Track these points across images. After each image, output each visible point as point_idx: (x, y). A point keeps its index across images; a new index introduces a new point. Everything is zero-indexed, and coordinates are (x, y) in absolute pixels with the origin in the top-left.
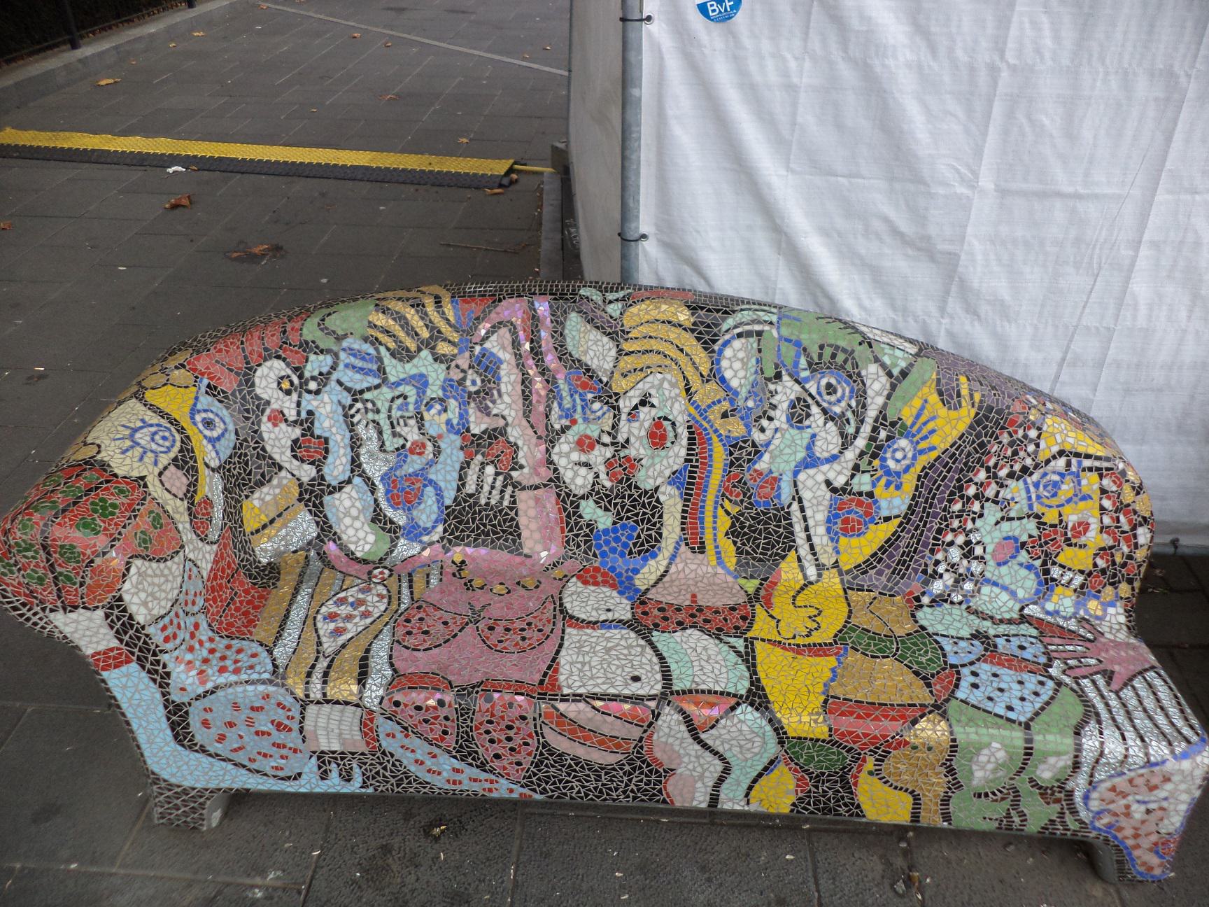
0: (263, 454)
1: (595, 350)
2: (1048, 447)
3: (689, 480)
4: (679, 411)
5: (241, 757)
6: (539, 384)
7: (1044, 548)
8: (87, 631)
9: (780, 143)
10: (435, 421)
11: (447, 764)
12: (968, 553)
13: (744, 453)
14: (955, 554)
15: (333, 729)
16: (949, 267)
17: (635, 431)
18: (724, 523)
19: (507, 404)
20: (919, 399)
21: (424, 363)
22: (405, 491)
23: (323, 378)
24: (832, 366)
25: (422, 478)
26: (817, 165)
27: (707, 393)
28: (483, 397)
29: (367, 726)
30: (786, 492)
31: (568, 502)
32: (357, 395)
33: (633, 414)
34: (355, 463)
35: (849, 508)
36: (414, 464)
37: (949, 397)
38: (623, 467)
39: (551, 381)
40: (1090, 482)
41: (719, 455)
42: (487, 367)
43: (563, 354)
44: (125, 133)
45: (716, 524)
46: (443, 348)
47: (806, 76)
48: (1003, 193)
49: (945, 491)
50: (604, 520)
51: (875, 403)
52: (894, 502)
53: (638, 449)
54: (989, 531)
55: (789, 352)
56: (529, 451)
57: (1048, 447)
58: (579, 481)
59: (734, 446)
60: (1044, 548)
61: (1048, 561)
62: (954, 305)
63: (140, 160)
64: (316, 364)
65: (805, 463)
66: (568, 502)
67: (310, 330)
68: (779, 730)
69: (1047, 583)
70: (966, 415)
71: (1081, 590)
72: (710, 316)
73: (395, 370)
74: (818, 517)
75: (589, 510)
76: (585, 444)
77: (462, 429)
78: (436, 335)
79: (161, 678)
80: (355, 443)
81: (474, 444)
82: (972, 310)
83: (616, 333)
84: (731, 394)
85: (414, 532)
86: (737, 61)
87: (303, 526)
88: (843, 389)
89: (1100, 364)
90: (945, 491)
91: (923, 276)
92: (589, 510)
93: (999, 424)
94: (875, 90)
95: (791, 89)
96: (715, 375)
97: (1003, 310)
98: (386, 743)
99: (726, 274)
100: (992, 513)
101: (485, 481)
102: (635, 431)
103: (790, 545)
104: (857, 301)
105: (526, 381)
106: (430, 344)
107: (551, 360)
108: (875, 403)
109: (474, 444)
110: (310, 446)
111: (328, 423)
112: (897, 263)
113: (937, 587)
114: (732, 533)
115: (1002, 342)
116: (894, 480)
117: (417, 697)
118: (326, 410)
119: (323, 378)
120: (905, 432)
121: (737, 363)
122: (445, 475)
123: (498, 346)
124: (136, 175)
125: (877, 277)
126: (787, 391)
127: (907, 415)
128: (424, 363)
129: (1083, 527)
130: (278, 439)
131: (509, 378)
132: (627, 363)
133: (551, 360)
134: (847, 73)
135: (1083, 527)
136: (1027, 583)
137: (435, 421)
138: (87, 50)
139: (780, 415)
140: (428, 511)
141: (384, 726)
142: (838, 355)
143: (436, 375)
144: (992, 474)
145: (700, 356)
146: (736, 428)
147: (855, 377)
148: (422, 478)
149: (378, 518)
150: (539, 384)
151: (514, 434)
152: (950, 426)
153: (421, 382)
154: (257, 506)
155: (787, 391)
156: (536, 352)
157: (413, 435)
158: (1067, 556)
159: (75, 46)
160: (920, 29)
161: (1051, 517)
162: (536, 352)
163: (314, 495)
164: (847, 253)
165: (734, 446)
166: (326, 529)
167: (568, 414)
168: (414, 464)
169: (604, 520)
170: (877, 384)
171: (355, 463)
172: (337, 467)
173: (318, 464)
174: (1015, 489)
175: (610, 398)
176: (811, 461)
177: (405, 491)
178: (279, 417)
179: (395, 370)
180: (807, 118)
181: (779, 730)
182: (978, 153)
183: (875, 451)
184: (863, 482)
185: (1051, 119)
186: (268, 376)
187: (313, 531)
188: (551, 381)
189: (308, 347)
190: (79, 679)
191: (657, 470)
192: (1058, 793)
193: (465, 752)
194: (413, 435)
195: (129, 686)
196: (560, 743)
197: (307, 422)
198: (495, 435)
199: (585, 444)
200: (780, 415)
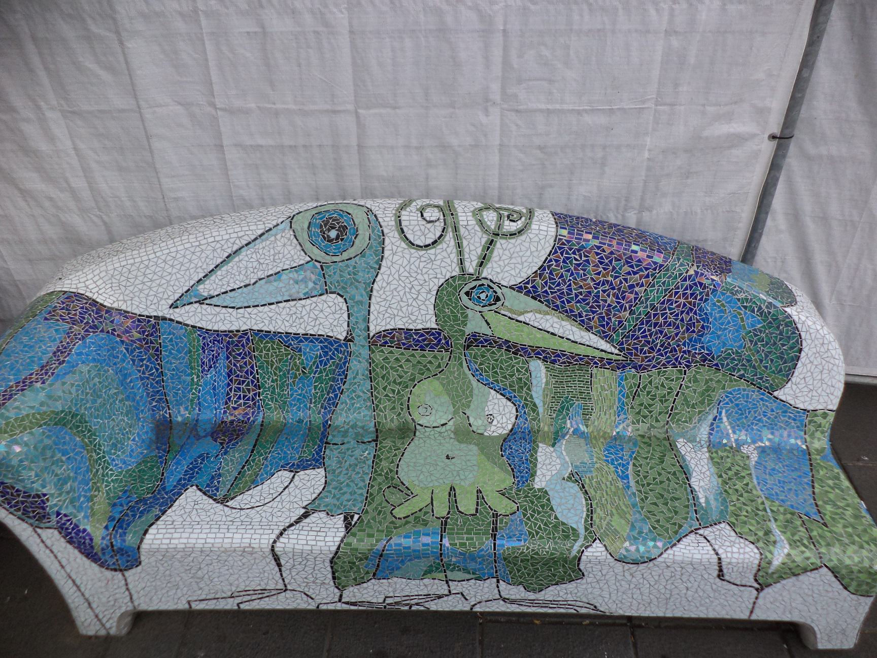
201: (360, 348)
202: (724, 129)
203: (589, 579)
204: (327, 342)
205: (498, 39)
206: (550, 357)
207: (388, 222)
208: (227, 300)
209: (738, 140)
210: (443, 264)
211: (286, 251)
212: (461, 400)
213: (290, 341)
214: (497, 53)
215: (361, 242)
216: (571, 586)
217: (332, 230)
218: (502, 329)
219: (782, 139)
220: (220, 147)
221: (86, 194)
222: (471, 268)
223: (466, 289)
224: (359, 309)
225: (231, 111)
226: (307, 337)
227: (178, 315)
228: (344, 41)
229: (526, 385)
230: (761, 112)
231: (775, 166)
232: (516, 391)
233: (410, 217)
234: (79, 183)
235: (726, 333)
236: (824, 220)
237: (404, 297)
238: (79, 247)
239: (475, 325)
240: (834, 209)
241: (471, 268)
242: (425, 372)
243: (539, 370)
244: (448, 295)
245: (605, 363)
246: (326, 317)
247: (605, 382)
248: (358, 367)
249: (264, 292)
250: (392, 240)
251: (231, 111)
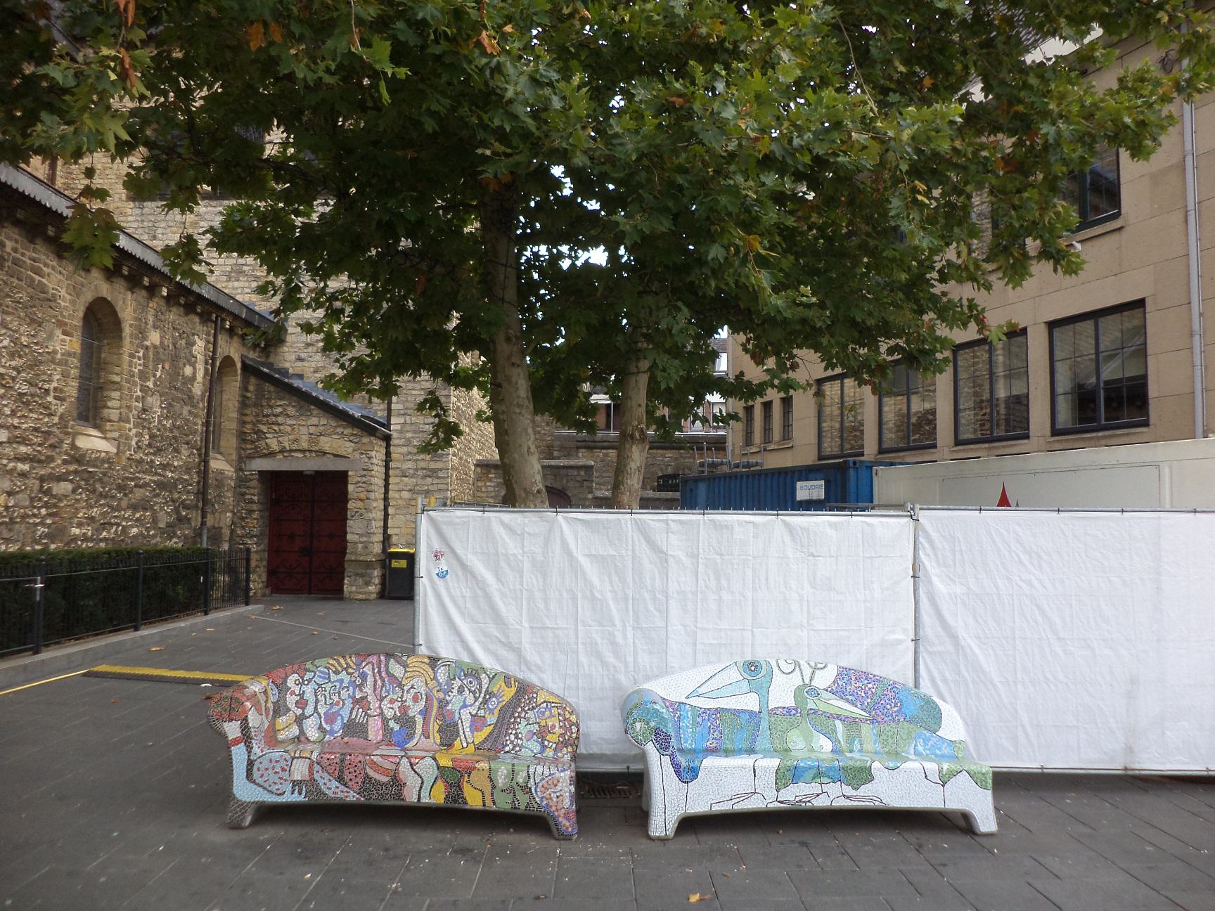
0: (286, 706)
1: (397, 670)
2: (540, 700)
3: (425, 713)
4: (423, 690)
5: (266, 785)
6: (379, 683)
7: (542, 733)
8: (232, 729)
9: (462, 614)
10: (344, 694)
11: (335, 783)
12: (517, 738)
13: (443, 704)
14: (512, 737)
15: (300, 771)
16: (517, 651)
17: (408, 697)
18: (437, 727)
19: (368, 689)
20: (499, 684)
21: (343, 675)
22: (331, 718)
23: (310, 680)
24: (471, 675)
25: (337, 714)
26: (474, 621)
27: (432, 684)
28: (361, 687)
29: (311, 768)
30: (457, 716)
31: (385, 721)
32: (320, 686)
33: (408, 691)
34: (316, 708)
35: (477, 722)
36: (336, 708)
37: (508, 685)
38: (404, 709)
39: (383, 681)
40: (555, 711)
41: (435, 704)
42: (363, 677)
43: (388, 672)
44: (176, 669)
45: (434, 727)
46: (350, 670)
47: (468, 594)
48: (532, 628)
49: (508, 715)
50: (397, 728)
51: (485, 687)
52: (491, 719)
53: (409, 703)
54: (523, 729)
55: (458, 671)
56: (374, 704)
57: (540, 700)
58: (389, 714)
59: (440, 701)
60: (542, 733)
61: (543, 739)
62: (523, 667)
63: (184, 681)
64: (309, 675)
65: (463, 708)
66: (385, 721)
67: (309, 665)
68: (438, 765)
69: (544, 747)
70: (514, 690)
71: (555, 750)
72: (434, 661)
73: (333, 677)
74: (467, 725)
75: (392, 724)
76: (392, 702)
77: (353, 697)
78: (349, 666)
79: (249, 749)
80: (317, 701)
81: (356, 702)
82: (530, 669)
83: (405, 666)
84: (440, 684)
85: (332, 732)
86: (448, 589)
87: (295, 731)
88: (475, 682)
89: (578, 689)
90: (508, 715)
91: (511, 656)
92: (392, 724)
93: (524, 690)
94: (488, 598)
95: (464, 597)
96: (435, 678)
97: (539, 668)
98: (316, 776)
99: (445, 652)
100: (524, 722)
101: (359, 715)
102: (408, 697)
103: (458, 735)
104: (487, 662)
105: (375, 681)
106: (346, 669)
107: (384, 674)
108: (485, 687)
109: (356, 702)
110: (302, 703)
111: (309, 695)
112: (503, 652)
113: (507, 749)
114: (439, 731)
115: (541, 679)
116: (491, 712)
117: (328, 756)
118: (309, 691)
119: (310, 680)
120: (495, 696)
121: (442, 675)
122: (345, 713)
123: (368, 670)
124: (182, 687)
125: (498, 659)
126: (457, 683)
127: (495, 690)
128: (343, 675)
129: (553, 726)
130: (291, 700)
131: (370, 680)
132: (408, 674)
133: (384, 674)
134: (479, 592)
135: (553, 726)
136: (537, 748)
137: (344, 694)
138: (145, 632)
139: (455, 691)
140: (338, 725)
141: (317, 767)
142: (474, 672)
143: (347, 679)
144: (523, 710)
145: (431, 672)
146: (441, 695)
147: (478, 679)
148: (337, 714)
149: (320, 728)
150: (379, 683)
151: (369, 698)
152: (509, 693)
153: (341, 681)
154: (281, 721)
155: (457, 683)
156: (379, 672)
157: (336, 698)
158: (549, 737)
159: (136, 629)
160: (499, 580)
161: (543, 723)
162: (379, 672)
163: (300, 720)
164: (486, 649)
165: (440, 701)
166: (302, 731)
167: (387, 691)
168: (336, 708)
169: (397, 728)
170: (485, 681)
171: (316, 708)
172: (309, 710)
173: (303, 709)
174: (530, 714)
175: (401, 686)
176: (465, 706)
177: (331, 718)
178: (293, 693)
179: (333, 677)
180: (469, 605)
181: (438, 765)
182: (521, 615)
183: (485, 702)
184: (481, 713)
185: (541, 605)
186: (291, 681)
187: (297, 733)
188: (383, 681)
189: (307, 670)
190: (226, 745)
191: (415, 710)
192: (525, 789)
193: (340, 779)
194: (336, 698)
195: (239, 754)
196: (371, 773)
197: (302, 695)
198: (364, 698)
199: (392, 702)
200: (455, 691)
201: (765, 715)
202: (892, 637)
203: (876, 780)
204: (751, 713)
205: (805, 603)
206: (844, 719)
207: (774, 664)
208: (709, 695)
209: (899, 642)
210: (796, 680)
211: (734, 675)
212: (808, 738)
213: (736, 713)
214: (805, 609)
215: (764, 672)
216: (869, 785)
217: (752, 667)
218: (822, 707)
219: (915, 640)
220: (695, 644)
221: (631, 665)
222: (807, 681)
223: (805, 691)
224: (764, 700)
225: (702, 629)
226: (744, 711)
227: (688, 701)
228: (750, 602)
229: (835, 731)
230: (905, 630)
231: (916, 653)
232: (831, 734)
233: (782, 663)
234: (630, 659)
235: (912, 708)
236: (945, 680)
237: (782, 694)
238: (648, 678)
239: (811, 705)
240: (947, 674)
241: (807, 681)
242: (792, 726)
243: (838, 722)
244: (798, 692)
245: (865, 721)
246: (750, 702)
247: (866, 729)
248: (764, 724)
249: (724, 692)
250: (776, 670)
251: (702, 629)
